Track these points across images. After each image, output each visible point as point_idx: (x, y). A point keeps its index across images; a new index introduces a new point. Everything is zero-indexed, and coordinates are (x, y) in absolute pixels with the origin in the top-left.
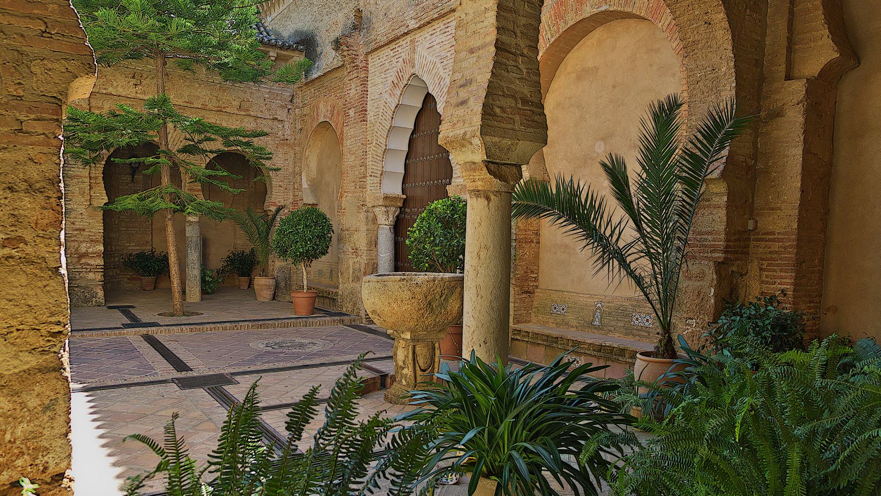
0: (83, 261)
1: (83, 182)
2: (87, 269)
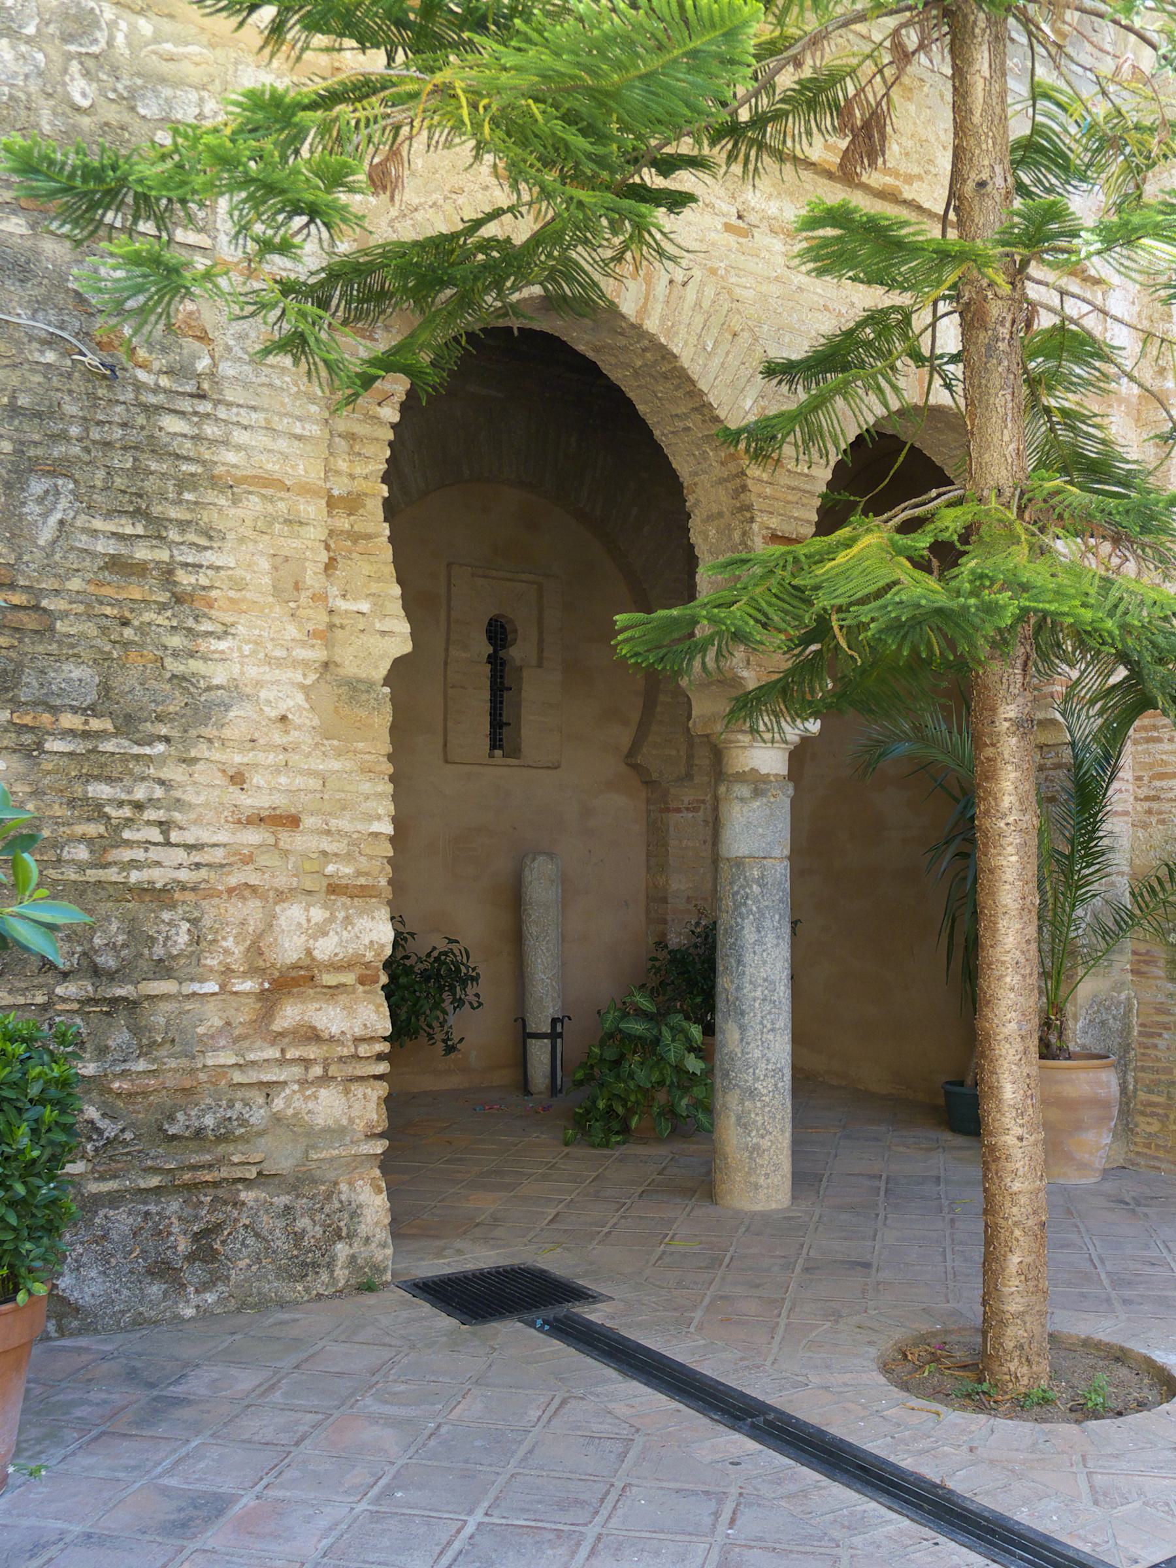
0: (290, 1014)
1: (294, 522)
2: (306, 1063)
